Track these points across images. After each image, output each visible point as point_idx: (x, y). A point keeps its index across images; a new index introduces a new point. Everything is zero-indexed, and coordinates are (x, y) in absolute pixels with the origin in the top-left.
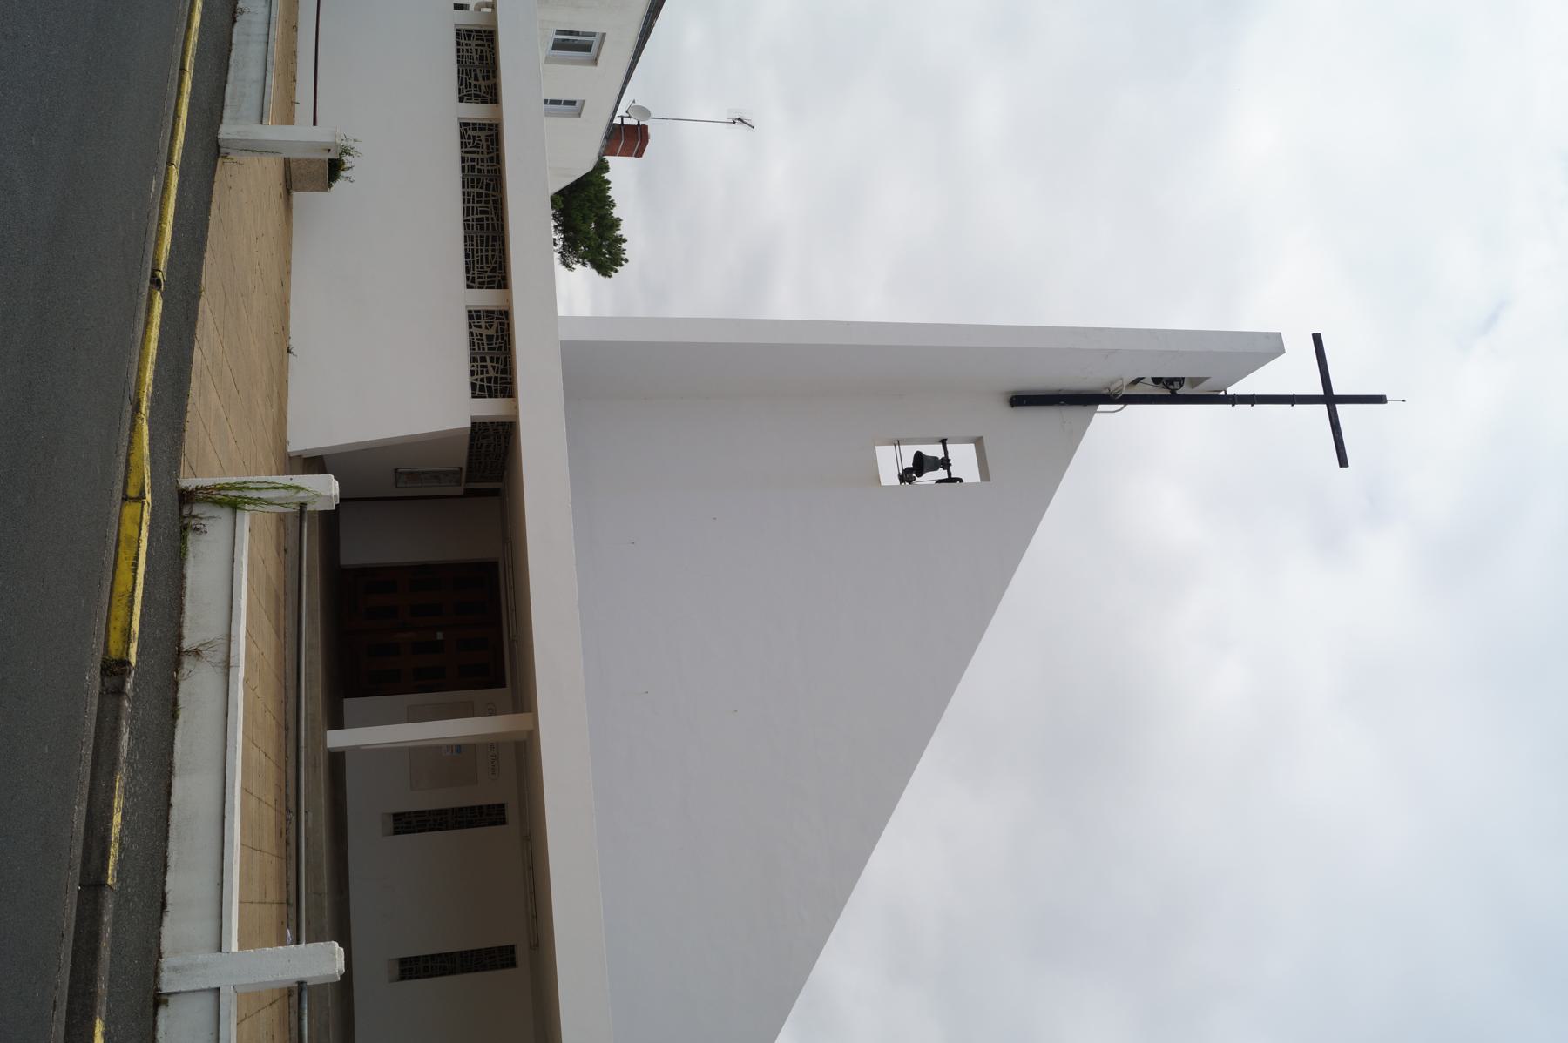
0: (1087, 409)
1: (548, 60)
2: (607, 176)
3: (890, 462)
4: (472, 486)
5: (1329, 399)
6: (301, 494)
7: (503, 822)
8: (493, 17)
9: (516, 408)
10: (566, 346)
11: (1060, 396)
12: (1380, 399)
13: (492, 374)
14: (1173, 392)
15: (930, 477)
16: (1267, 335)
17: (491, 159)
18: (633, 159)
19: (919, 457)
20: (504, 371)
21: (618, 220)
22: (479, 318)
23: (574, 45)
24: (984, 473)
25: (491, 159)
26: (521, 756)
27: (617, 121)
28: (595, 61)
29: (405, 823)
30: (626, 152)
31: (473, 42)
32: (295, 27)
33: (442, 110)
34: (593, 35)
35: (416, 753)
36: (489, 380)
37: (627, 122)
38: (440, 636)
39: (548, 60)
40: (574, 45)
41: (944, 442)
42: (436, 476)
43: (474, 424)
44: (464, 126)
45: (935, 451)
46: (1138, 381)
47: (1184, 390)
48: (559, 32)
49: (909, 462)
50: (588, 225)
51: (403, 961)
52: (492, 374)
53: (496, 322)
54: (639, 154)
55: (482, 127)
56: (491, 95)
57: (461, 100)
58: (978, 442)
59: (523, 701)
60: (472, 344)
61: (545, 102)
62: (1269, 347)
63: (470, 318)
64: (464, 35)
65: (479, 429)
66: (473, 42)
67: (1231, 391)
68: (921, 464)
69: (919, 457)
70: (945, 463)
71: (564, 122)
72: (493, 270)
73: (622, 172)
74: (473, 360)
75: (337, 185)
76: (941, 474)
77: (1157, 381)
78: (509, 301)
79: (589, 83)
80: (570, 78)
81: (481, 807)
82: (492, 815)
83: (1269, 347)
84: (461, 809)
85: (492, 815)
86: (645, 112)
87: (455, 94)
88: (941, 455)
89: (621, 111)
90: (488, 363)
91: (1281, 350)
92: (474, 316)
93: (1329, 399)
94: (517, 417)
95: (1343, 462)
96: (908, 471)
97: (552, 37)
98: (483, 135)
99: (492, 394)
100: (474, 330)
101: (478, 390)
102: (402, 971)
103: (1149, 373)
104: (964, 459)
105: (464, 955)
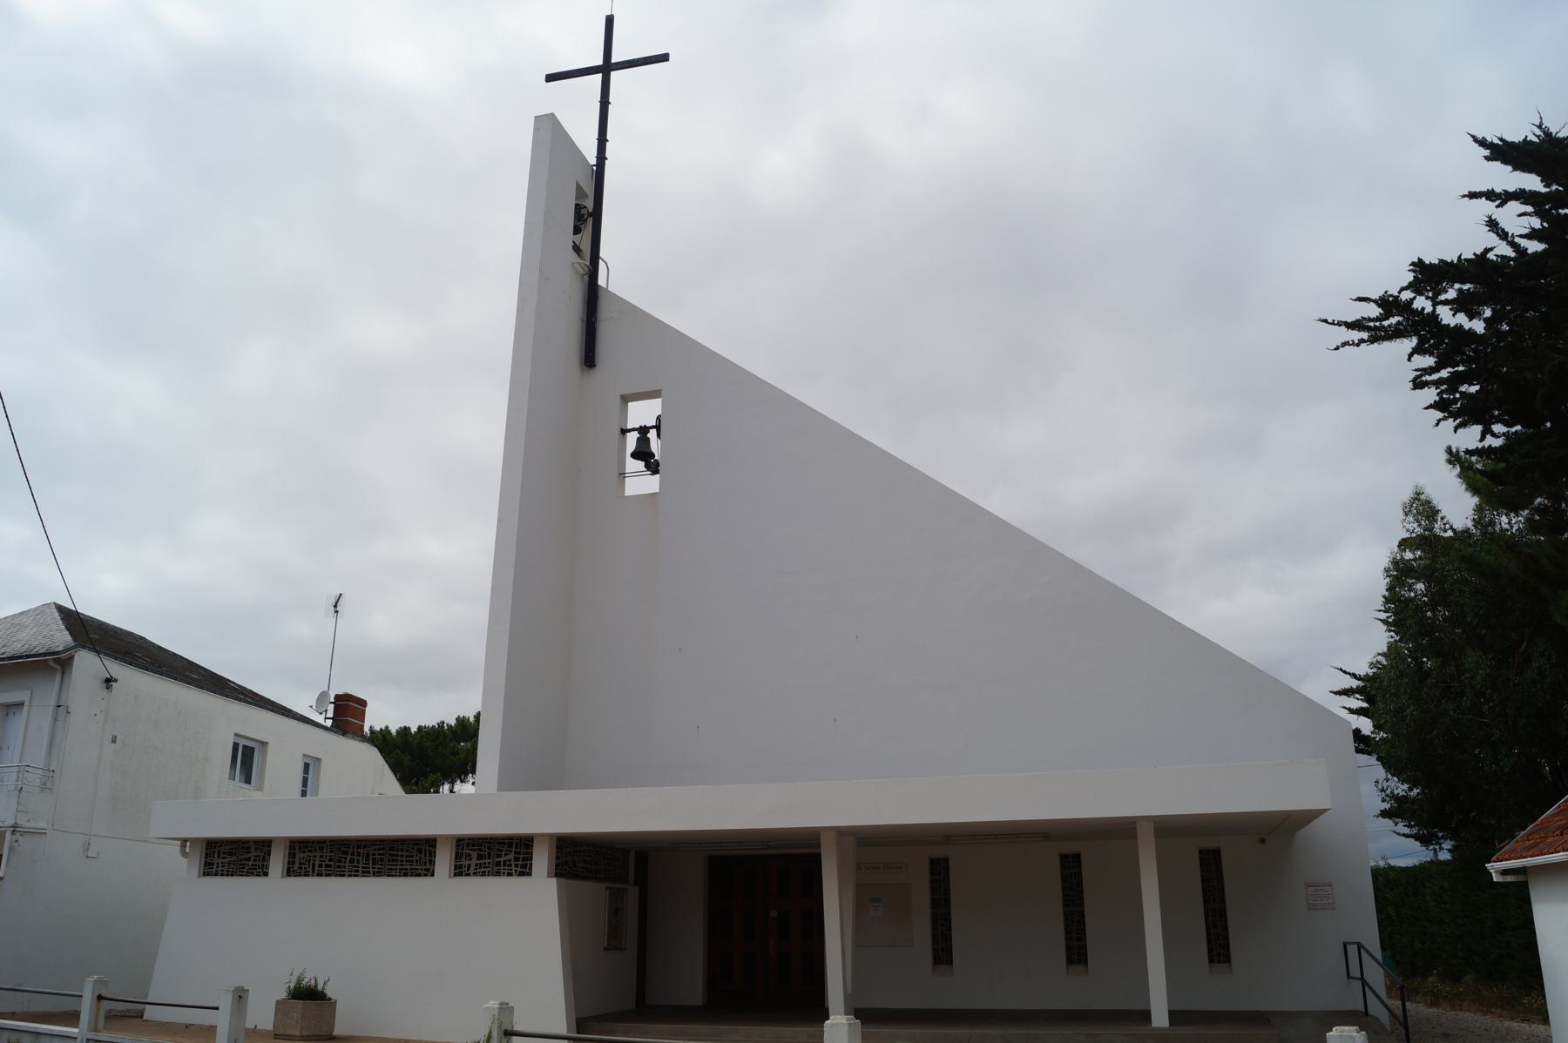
0: (601, 295)
1: (260, 789)
2: (414, 729)
3: (640, 483)
4: (631, 878)
5: (607, 68)
6: (495, 1034)
7: (946, 860)
8: (194, 841)
9: (542, 835)
10: (500, 789)
11: (582, 322)
12: (610, 21)
13: (511, 856)
14: (590, 215)
15: (655, 445)
16: (536, 129)
17: (321, 849)
18: (368, 710)
19: (635, 455)
20: (510, 845)
21: (458, 719)
22: (461, 866)
23: (245, 758)
24: (654, 394)
25: (321, 849)
26: (872, 846)
27: (329, 723)
28: (264, 744)
29: (942, 954)
30: (361, 715)
31: (216, 861)
32: (187, 1026)
33: (276, 891)
34: (236, 746)
35: (861, 939)
36: (516, 859)
37: (330, 714)
38: (774, 914)
39: (260, 789)
40: (245, 758)
41: (624, 432)
42: (616, 912)
43: (557, 875)
44: (290, 872)
45: (632, 440)
46: (577, 249)
47: (589, 204)
48: (232, 777)
49: (640, 465)
50: (431, 757)
51: (1070, 961)
52: (511, 856)
53: (466, 851)
54: (363, 703)
55: (292, 855)
56: (264, 845)
57: (266, 874)
58: (626, 399)
59: (1121, 831)
60: (484, 874)
61: (304, 794)
62: (549, 130)
63: (460, 874)
64: (209, 869)
65: (562, 870)
66: (216, 861)
67: (593, 161)
68: (643, 453)
69: (635, 455)
70: (643, 431)
71: (327, 779)
72: (420, 851)
73: (377, 717)
74: (498, 874)
75: (329, 993)
76: (652, 434)
77: (577, 230)
78: (447, 838)
79: (284, 748)
80: (280, 769)
81: (932, 881)
82: (939, 871)
83: (549, 130)
84: (933, 900)
85: (939, 871)
86: (323, 696)
87: (524, 879)
88: (635, 435)
89: (320, 719)
90: (502, 859)
91: (551, 118)
92: (459, 871)
93: (607, 68)
94: (551, 835)
95: (664, 58)
96: (648, 466)
97: (238, 784)
98: (299, 855)
99: (529, 858)
100: (472, 871)
101: (525, 870)
102: (1080, 962)
103: (569, 237)
104: (642, 413)
105: (1067, 903)
